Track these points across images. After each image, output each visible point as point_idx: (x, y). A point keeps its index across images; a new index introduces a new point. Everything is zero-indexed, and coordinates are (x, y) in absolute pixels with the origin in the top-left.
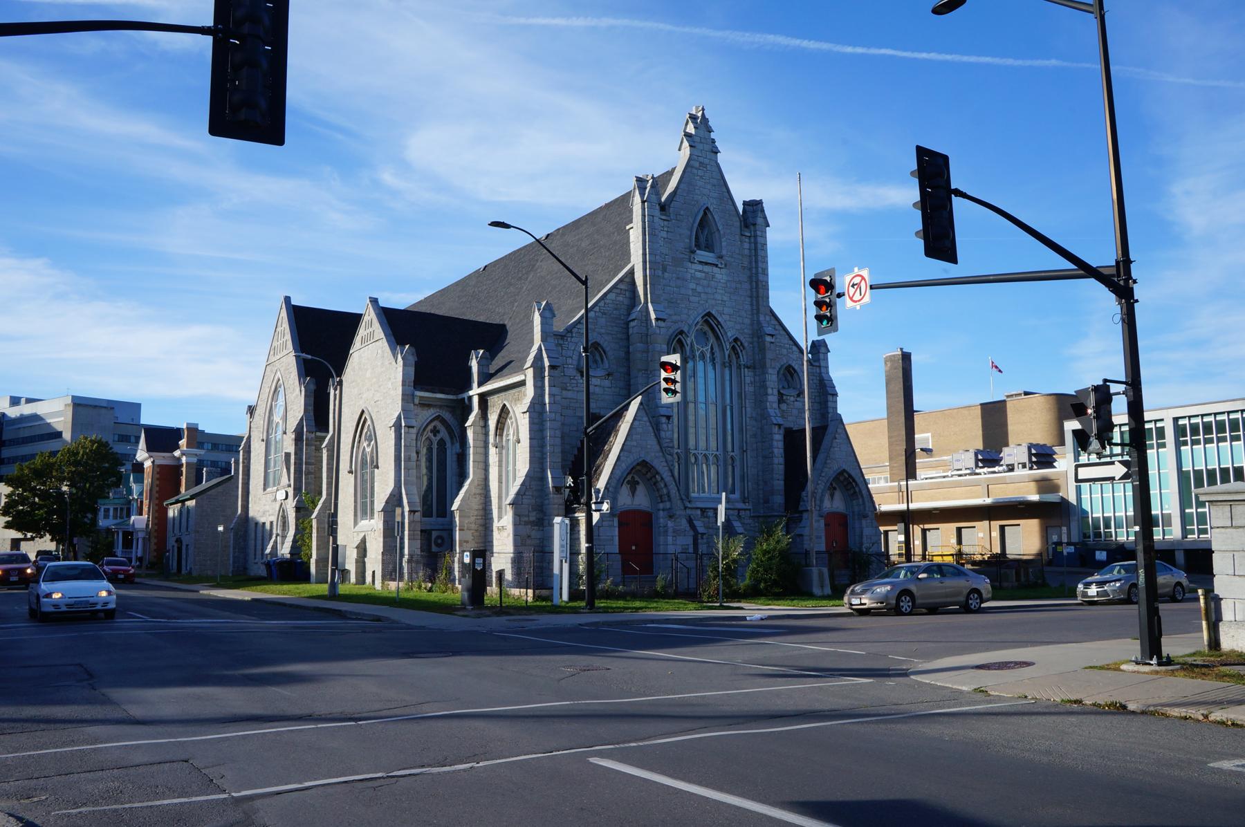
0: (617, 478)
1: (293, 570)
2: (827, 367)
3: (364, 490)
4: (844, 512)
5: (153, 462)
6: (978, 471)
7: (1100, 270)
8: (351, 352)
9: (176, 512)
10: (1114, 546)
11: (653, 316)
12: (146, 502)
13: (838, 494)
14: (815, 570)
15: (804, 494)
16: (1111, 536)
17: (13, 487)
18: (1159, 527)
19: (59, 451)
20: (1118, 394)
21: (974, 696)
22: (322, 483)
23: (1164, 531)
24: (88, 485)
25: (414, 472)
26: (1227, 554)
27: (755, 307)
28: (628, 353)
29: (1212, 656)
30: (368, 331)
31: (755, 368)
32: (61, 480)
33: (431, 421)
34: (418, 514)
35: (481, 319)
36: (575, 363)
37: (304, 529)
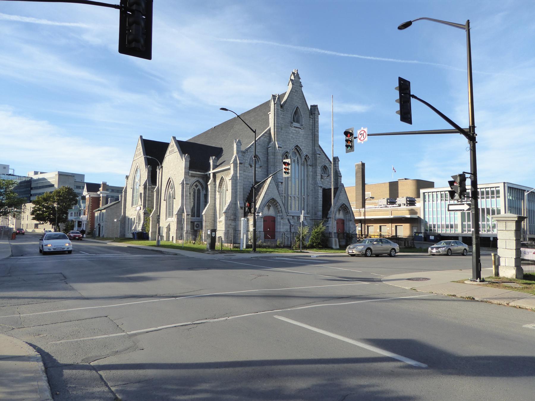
0: (263, 204)
1: (142, 236)
2: (338, 167)
3: (169, 207)
4: (343, 218)
5: (90, 196)
6: (388, 206)
7: (464, 129)
8: (165, 156)
9: (98, 214)
10: (437, 234)
11: (277, 146)
12: (87, 211)
13: (341, 212)
14: (333, 239)
15: (329, 212)
16: (436, 231)
17: (35, 205)
18: (453, 228)
19: (53, 192)
20: (468, 178)
21: (411, 291)
22: (154, 204)
23: (442, 230)
24: (64, 204)
25: (189, 200)
26: (503, 240)
27: (313, 144)
28: (268, 159)
29: (497, 278)
30: (172, 149)
31: (313, 166)
32: (54, 202)
33: (195, 182)
34: (190, 216)
35: (214, 146)
36: (249, 162)
37: (147, 220)
